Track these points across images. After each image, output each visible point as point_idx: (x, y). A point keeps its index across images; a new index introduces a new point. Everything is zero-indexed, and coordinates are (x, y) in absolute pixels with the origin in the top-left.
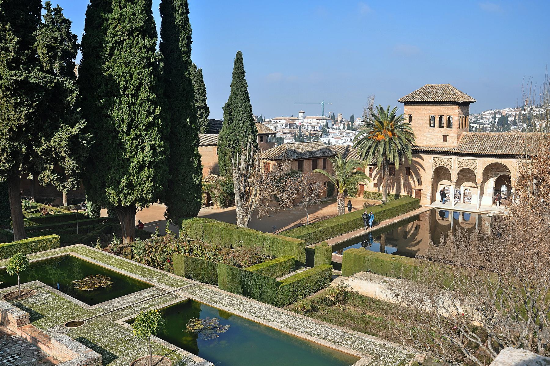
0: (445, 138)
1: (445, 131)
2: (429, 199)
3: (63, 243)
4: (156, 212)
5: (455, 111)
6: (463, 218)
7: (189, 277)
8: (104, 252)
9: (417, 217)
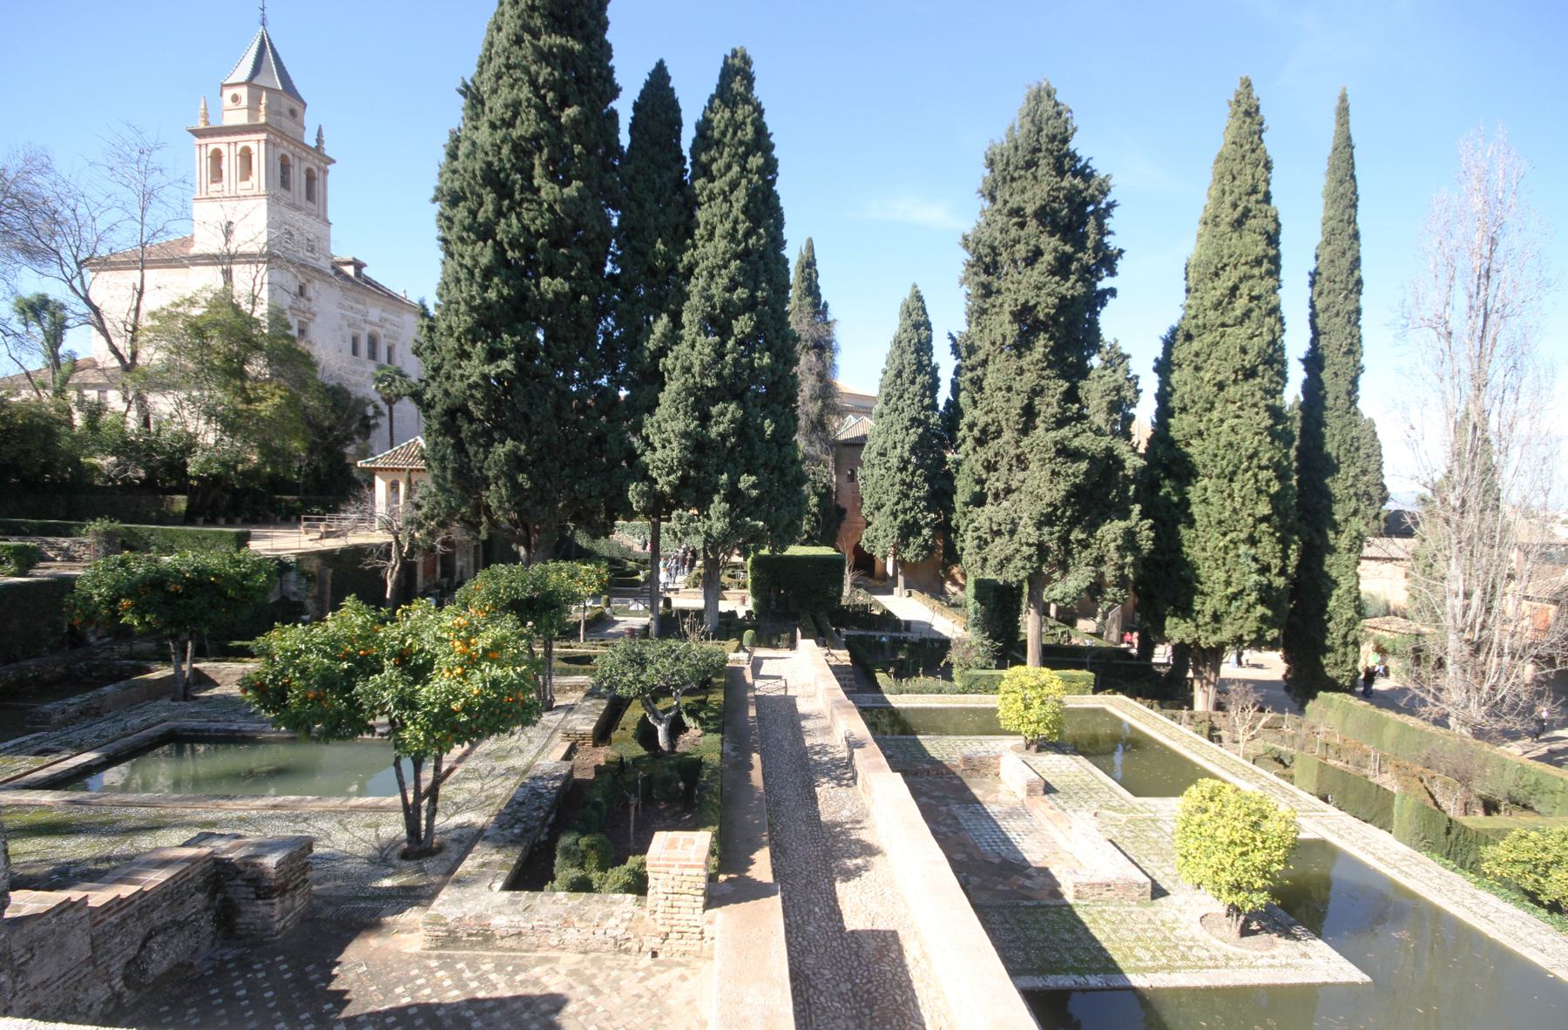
3: (1098, 688)
7: (1325, 799)
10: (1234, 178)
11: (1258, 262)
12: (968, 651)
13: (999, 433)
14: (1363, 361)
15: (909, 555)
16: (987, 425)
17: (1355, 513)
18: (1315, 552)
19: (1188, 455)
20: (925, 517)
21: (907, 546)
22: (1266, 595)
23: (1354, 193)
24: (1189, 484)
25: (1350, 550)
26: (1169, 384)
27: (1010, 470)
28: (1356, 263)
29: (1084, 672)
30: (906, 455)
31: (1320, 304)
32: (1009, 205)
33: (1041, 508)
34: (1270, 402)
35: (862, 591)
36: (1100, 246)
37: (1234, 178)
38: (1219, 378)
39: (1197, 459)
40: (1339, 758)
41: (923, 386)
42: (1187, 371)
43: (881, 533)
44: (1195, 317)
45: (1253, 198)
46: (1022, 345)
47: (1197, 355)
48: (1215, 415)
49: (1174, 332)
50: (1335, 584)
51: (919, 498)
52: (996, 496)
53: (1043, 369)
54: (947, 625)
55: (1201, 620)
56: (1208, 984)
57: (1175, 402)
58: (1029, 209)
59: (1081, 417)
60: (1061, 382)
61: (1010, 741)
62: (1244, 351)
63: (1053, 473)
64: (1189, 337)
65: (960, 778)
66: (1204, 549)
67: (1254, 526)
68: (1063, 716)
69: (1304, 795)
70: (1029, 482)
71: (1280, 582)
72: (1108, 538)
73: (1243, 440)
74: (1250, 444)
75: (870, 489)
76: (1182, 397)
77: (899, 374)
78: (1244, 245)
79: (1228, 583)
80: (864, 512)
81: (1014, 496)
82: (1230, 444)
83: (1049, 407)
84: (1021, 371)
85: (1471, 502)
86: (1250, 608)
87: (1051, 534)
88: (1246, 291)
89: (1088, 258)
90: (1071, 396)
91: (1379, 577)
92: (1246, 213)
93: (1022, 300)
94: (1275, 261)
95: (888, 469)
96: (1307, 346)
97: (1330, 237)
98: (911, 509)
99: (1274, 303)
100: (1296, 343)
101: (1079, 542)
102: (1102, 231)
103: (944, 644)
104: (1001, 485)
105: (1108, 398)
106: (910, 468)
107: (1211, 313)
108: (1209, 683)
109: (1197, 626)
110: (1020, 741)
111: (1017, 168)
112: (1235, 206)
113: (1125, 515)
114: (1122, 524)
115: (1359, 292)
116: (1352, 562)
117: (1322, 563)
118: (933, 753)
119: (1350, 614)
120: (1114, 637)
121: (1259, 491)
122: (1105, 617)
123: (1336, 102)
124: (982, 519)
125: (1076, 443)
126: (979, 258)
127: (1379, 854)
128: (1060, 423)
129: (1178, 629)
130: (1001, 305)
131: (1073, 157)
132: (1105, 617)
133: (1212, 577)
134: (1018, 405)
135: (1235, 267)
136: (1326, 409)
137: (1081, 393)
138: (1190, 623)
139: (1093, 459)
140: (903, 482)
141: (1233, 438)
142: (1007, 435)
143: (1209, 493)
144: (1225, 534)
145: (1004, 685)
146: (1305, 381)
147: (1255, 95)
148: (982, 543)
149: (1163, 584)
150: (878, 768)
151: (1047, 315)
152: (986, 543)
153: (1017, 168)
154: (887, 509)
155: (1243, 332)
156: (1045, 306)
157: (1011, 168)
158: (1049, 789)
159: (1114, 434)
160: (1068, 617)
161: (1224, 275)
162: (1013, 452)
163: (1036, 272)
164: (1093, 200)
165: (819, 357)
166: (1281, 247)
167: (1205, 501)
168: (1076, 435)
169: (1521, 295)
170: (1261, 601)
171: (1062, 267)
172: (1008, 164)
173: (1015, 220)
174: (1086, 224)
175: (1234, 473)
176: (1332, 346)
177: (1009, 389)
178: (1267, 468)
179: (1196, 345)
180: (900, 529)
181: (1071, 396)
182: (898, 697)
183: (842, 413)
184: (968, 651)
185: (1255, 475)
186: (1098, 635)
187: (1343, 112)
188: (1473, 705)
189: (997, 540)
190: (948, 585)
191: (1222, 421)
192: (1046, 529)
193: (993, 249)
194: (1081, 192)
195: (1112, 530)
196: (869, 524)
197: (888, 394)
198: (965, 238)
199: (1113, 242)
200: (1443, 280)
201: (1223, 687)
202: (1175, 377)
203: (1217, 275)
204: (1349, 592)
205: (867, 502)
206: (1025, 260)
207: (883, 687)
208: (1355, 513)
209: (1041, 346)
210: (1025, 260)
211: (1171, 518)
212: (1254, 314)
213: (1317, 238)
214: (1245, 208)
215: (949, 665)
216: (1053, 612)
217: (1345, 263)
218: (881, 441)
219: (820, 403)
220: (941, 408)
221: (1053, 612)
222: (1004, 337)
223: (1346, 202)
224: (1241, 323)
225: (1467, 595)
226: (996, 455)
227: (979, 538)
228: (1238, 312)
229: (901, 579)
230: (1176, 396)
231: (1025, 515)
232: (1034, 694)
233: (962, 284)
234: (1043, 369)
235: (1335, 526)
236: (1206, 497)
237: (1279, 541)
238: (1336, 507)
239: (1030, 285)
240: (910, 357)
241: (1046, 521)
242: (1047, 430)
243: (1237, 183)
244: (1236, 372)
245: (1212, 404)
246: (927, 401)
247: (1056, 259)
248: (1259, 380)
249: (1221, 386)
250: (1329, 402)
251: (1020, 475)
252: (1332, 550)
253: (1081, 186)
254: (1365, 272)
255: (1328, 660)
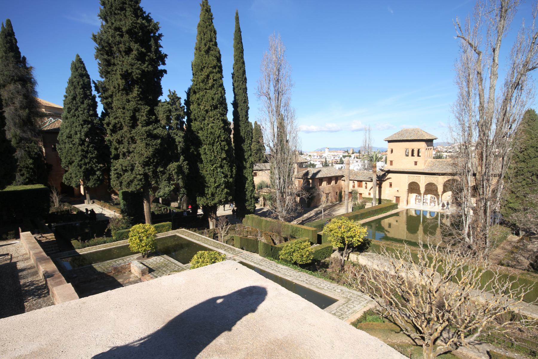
0: (416, 163)
1: (416, 158)
2: (405, 203)
3: (174, 228)
4: (225, 210)
5: (423, 145)
6: (430, 215)
7: (243, 249)
8: (203, 236)
9: (397, 214)
10: (204, 35)
11: (215, 67)
12: (118, 223)
13: (121, 128)
14: (249, 105)
15: (90, 184)
16: (116, 124)
17: (251, 155)
18: (241, 169)
19: (198, 137)
20: (97, 166)
21: (89, 180)
22: (227, 185)
23: (242, 48)
24: (200, 147)
25: (250, 168)
26: (190, 110)
27: (129, 143)
28: (244, 72)
29: (168, 223)
30: (83, 137)
31: (236, 85)
32: (114, 25)
33: (143, 159)
34: (223, 118)
35: (66, 204)
36: (157, 52)
37: (204, 35)
38: (206, 108)
39: (201, 138)
40: (251, 235)
41: (88, 105)
42: (196, 105)
43: (73, 175)
44: (196, 85)
45: (211, 43)
46: (127, 90)
47: (198, 99)
48: (206, 122)
49: (190, 89)
50: (247, 179)
51: (93, 158)
52: (124, 155)
53: (138, 101)
54: (109, 213)
55: (208, 197)
56: (241, 320)
57: (192, 117)
58: (124, 29)
59: (157, 121)
60: (146, 107)
61: (136, 256)
62: (213, 99)
63: (147, 144)
64: (195, 93)
65: (113, 277)
66: (207, 171)
67: (222, 162)
68: (155, 243)
69: (237, 249)
70: (137, 148)
71: (231, 180)
72: (172, 169)
73: (215, 131)
74: (218, 132)
75: (64, 155)
76: (194, 115)
77: (74, 98)
78: (210, 60)
79: (215, 182)
80: (63, 166)
81: (132, 154)
82: (211, 133)
83: (142, 117)
84: (128, 101)
85: (279, 150)
86: (223, 190)
87: (149, 169)
88: (212, 78)
89: (152, 55)
90: (151, 112)
91: (261, 177)
92: (209, 48)
93: (125, 69)
94: (220, 67)
95: (74, 144)
96: (233, 99)
97: (236, 62)
98: (89, 163)
99: (221, 82)
100: (230, 98)
101: (161, 172)
102: (158, 46)
103: (106, 220)
104: (125, 150)
105: (166, 114)
106: (86, 144)
107: (201, 84)
108: (213, 218)
109: (207, 199)
110: (140, 255)
111: (116, 9)
112: (205, 45)
113: (178, 160)
114: (177, 164)
115: (246, 82)
116: (251, 171)
117: (243, 172)
118: (99, 270)
119: (251, 188)
120: (185, 208)
121: (222, 149)
122: (181, 200)
123: (235, 15)
124: (117, 165)
125: (155, 132)
126: (103, 47)
127: (255, 261)
128: (148, 123)
129: (201, 201)
130: (116, 71)
131: (141, 10)
132: (181, 200)
133: (210, 180)
134: (129, 115)
135: (208, 68)
136: (240, 121)
137: (156, 112)
138: (205, 198)
139: (162, 138)
140: (83, 150)
141: (212, 131)
142: (125, 128)
143: (206, 151)
144: (213, 165)
145: (131, 234)
146: (234, 111)
147: (209, 4)
148: (119, 176)
149: (195, 185)
150: (60, 283)
151: (137, 77)
152: (121, 175)
153: (116, 9)
154: (75, 163)
155: (213, 92)
156: (136, 73)
157: (113, 8)
158: (151, 270)
159: (177, 128)
160: (167, 202)
161: (205, 70)
162: (129, 136)
163: (130, 58)
164: (152, 31)
165: (24, 86)
166: (222, 63)
167: (205, 153)
168: (155, 129)
169: (286, 88)
170: (226, 187)
171: (141, 57)
172: (112, 6)
173: (118, 33)
174: (150, 41)
175: (213, 143)
176: (240, 98)
177: (124, 108)
178: (223, 141)
179: (198, 96)
180: (84, 172)
181: (151, 112)
182: (83, 249)
183: (43, 115)
184: (118, 223)
185: (220, 144)
186: (179, 208)
187: (237, 19)
188: (283, 211)
189: (126, 174)
190: (113, 196)
191: (208, 124)
192: (146, 168)
193: (109, 44)
194: (146, 27)
195: (173, 166)
196: (67, 171)
197: (69, 108)
198: (94, 36)
199: (163, 51)
200: (267, 81)
201: (217, 219)
202: (192, 107)
203: (202, 70)
204: (251, 181)
205: (64, 161)
206: (125, 52)
207: (75, 246)
208: (251, 155)
209: (136, 91)
210: (125, 52)
211: (194, 160)
212: (215, 86)
213: (233, 62)
214: (208, 46)
215: (109, 231)
216: (160, 201)
217: (241, 71)
218: (68, 131)
219: (27, 111)
220: (99, 116)
221: (160, 201)
222: (119, 85)
223: (240, 51)
224: (211, 89)
225: (280, 179)
226: (122, 137)
227: (117, 173)
228: (210, 85)
229: (88, 196)
230: (192, 114)
231: (137, 162)
232: (143, 235)
233: (96, 59)
234: (138, 101)
235: (245, 160)
236: (206, 152)
237: (230, 166)
238: (245, 154)
239: (125, 63)
240: (79, 90)
241: (146, 164)
242: (142, 126)
243: (205, 36)
244: (211, 106)
245: (205, 118)
246: (91, 112)
247: (138, 53)
248: (218, 110)
249: (207, 111)
250: (241, 119)
251: (133, 146)
252: (245, 168)
253: (146, 24)
254: (248, 75)
255: (247, 204)
